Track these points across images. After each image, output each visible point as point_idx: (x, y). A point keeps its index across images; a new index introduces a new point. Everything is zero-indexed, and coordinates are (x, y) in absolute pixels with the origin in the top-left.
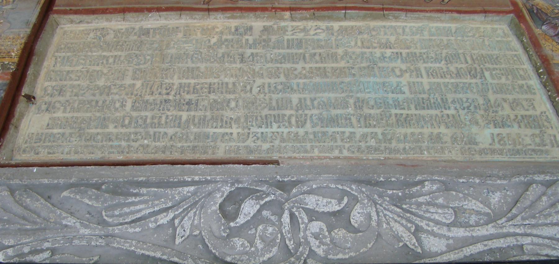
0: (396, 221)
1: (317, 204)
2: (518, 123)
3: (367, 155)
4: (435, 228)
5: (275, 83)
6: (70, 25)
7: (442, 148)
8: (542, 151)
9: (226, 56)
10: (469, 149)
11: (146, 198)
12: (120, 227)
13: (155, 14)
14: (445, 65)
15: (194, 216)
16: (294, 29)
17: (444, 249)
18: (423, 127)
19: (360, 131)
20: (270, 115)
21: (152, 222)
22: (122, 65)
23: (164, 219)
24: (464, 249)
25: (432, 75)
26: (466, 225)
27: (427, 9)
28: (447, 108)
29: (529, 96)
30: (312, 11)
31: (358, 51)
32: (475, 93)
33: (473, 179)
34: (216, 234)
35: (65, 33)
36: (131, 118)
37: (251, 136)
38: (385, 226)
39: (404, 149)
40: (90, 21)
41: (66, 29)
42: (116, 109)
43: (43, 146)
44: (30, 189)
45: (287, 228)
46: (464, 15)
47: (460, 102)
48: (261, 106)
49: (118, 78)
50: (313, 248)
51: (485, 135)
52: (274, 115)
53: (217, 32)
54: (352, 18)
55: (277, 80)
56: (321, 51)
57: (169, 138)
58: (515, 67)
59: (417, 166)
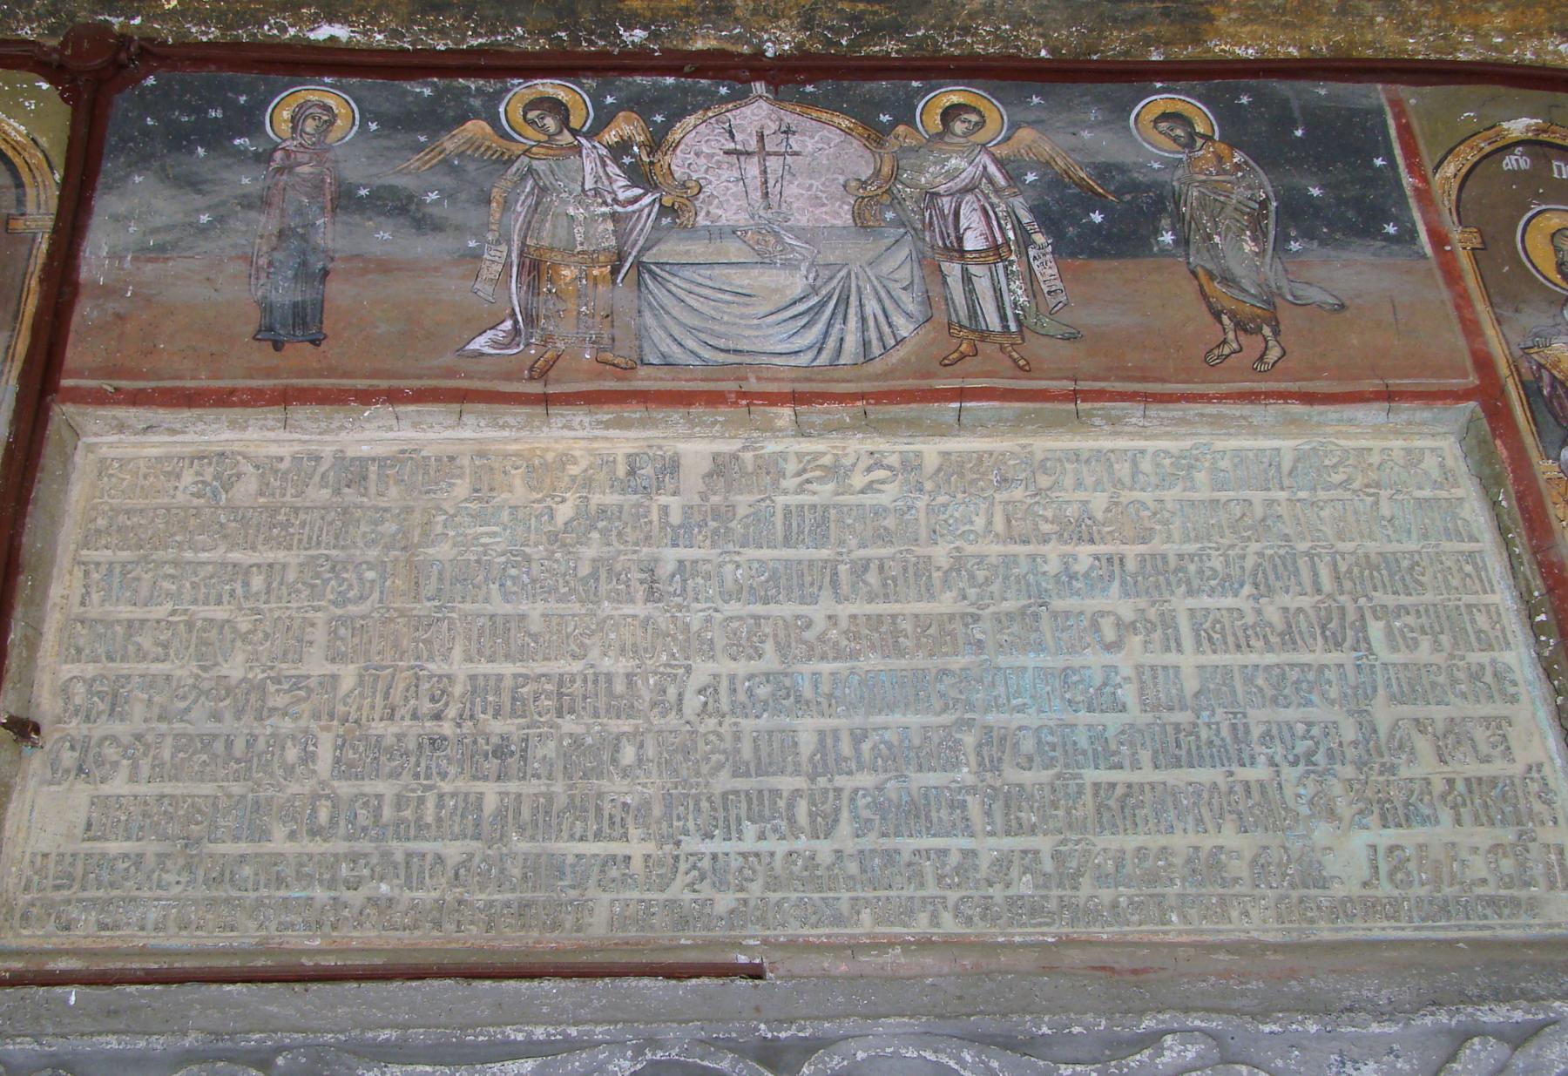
2: (1454, 807)
3: (1009, 930)
5: (750, 677)
6: (115, 438)
8: (1515, 903)
9: (603, 574)
13: (383, 411)
14: (1251, 602)
19: (991, 847)
20: (736, 793)
22: (294, 605)
25: (1210, 639)
27: (1211, 389)
28: (1247, 761)
30: (859, 403)
33: (1302, 1023)
35: (103, 466)
36: (335, 800)
37: (683, 866)
40: (178, 426)
42: (290, 770)
43: (80, 901)
46: (1322, 408)
47: (1286, 735)
48: (709, 759)
49: (285, 653)
51: (1350, 851)
52: (747, 794)
53: (573, 479)
54: (978, 426)
55: (756, 666)
57: (451, 874)
58: (1468, 599)
59: (1145, 971)
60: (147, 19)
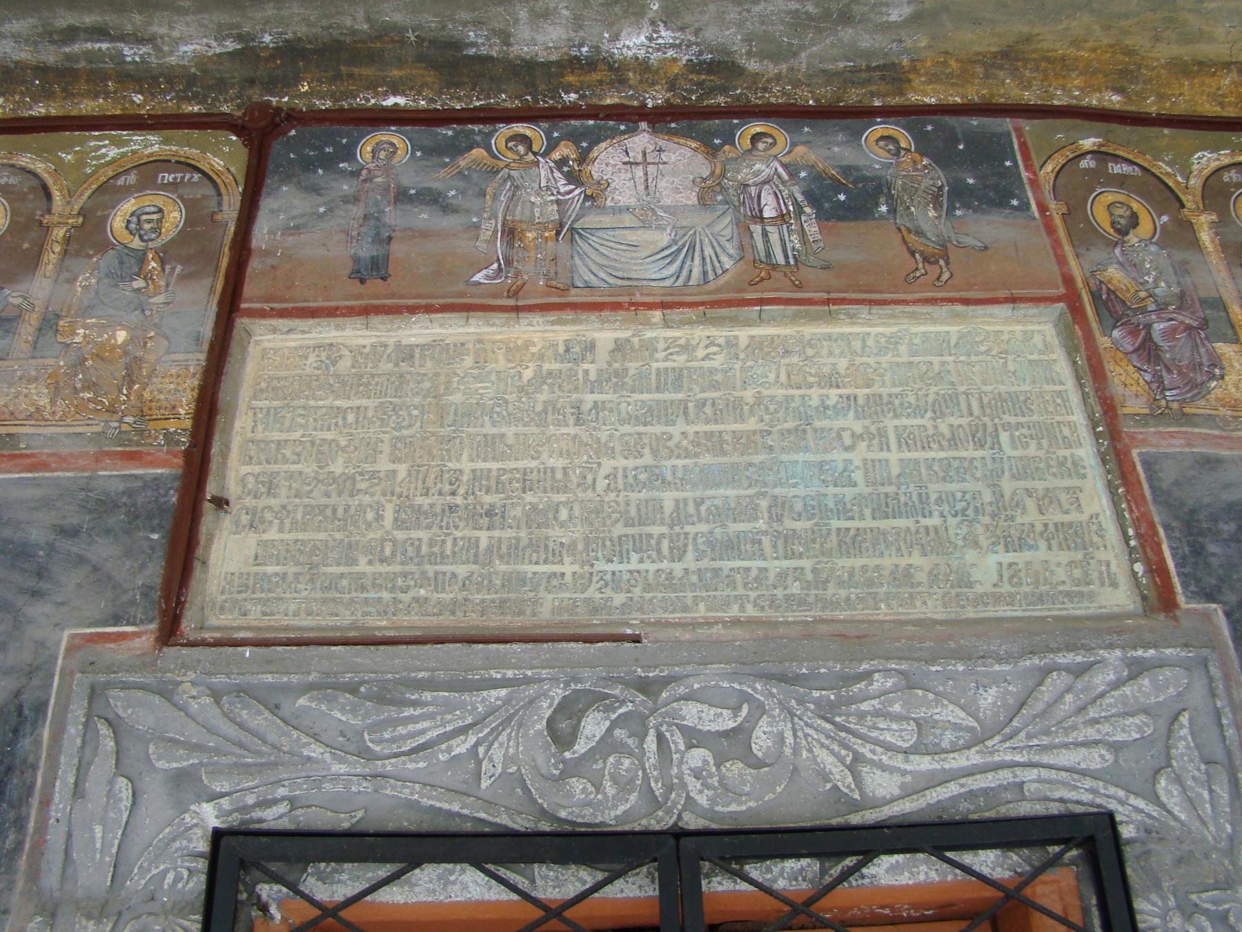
0: (822, 745)
1: (700, 718)
2: (1048, 540)
4: (884, 757)
5: (636, 469)
7: (911, 595)
8: (1081, 594)
10: (957, 595)
11: (431, 709)
12: (394, 760)
13: (422, 318)
15: (509, 740)
16: (670, 343)
17: (897, 792)
18: (882, 555)
19: (775, 566)
20: (626, 536)
21: (442, 752)
23: (461, 746)
24: (927, 792)
26: (935, 751)
27: (909, 297)
29: (1075, 482)
31: (780, 392)
32: (978, 480)
34: (544, 771)
36: (394, 542)
37: (595, 579)
38: (805, 754)
39: (848, 599)
41: (265, 344)
42: (369, 525)
44: (246, 693)
45: (652, 761)
47: (951, 499)
50: (691, 794)
51: (986, 567)
52: (633, 536)
53: (533, 354)
54: (773, 320)
56: (715, 395)
58: (1058, 418)
59: (864, 636)
60: (292, 97)
